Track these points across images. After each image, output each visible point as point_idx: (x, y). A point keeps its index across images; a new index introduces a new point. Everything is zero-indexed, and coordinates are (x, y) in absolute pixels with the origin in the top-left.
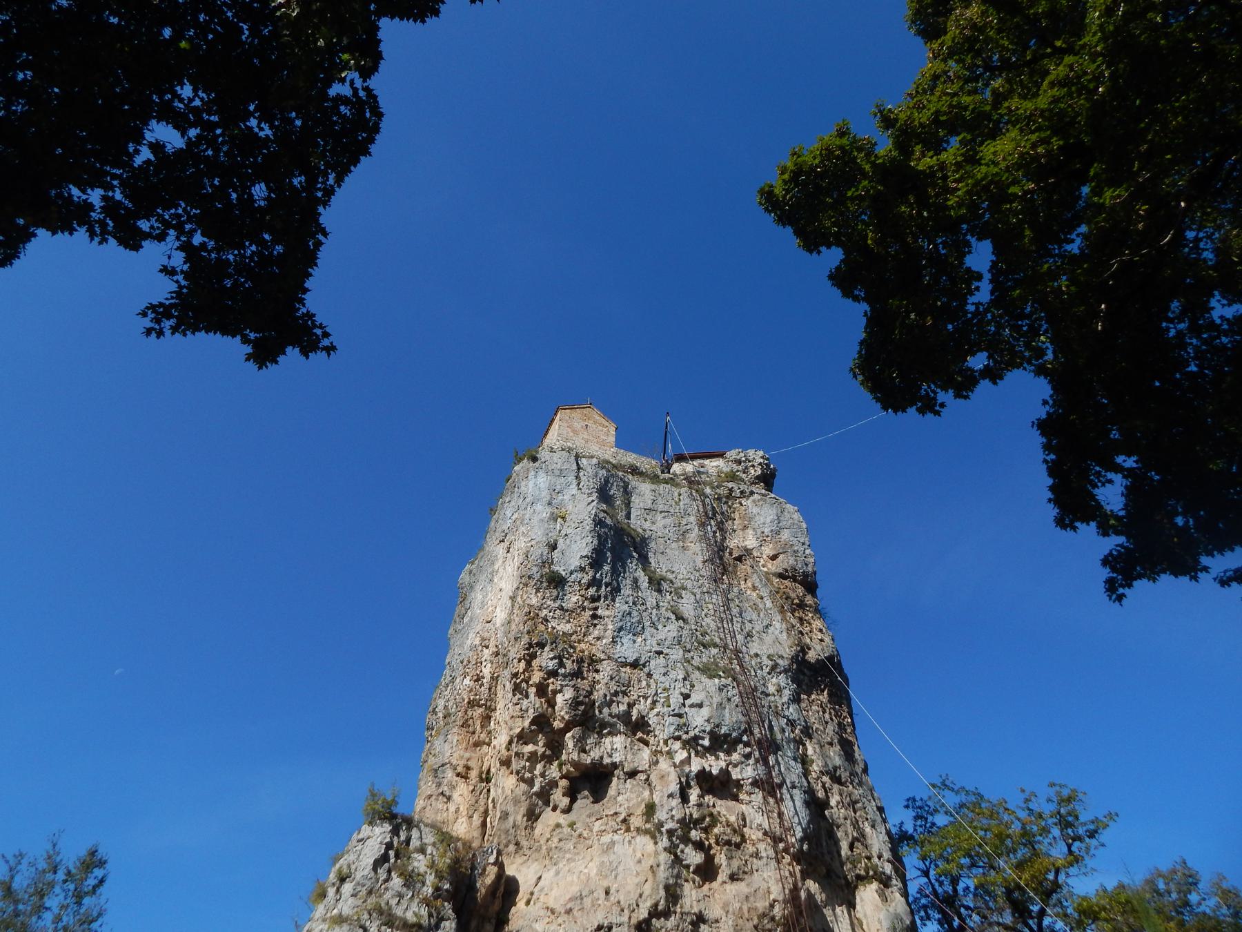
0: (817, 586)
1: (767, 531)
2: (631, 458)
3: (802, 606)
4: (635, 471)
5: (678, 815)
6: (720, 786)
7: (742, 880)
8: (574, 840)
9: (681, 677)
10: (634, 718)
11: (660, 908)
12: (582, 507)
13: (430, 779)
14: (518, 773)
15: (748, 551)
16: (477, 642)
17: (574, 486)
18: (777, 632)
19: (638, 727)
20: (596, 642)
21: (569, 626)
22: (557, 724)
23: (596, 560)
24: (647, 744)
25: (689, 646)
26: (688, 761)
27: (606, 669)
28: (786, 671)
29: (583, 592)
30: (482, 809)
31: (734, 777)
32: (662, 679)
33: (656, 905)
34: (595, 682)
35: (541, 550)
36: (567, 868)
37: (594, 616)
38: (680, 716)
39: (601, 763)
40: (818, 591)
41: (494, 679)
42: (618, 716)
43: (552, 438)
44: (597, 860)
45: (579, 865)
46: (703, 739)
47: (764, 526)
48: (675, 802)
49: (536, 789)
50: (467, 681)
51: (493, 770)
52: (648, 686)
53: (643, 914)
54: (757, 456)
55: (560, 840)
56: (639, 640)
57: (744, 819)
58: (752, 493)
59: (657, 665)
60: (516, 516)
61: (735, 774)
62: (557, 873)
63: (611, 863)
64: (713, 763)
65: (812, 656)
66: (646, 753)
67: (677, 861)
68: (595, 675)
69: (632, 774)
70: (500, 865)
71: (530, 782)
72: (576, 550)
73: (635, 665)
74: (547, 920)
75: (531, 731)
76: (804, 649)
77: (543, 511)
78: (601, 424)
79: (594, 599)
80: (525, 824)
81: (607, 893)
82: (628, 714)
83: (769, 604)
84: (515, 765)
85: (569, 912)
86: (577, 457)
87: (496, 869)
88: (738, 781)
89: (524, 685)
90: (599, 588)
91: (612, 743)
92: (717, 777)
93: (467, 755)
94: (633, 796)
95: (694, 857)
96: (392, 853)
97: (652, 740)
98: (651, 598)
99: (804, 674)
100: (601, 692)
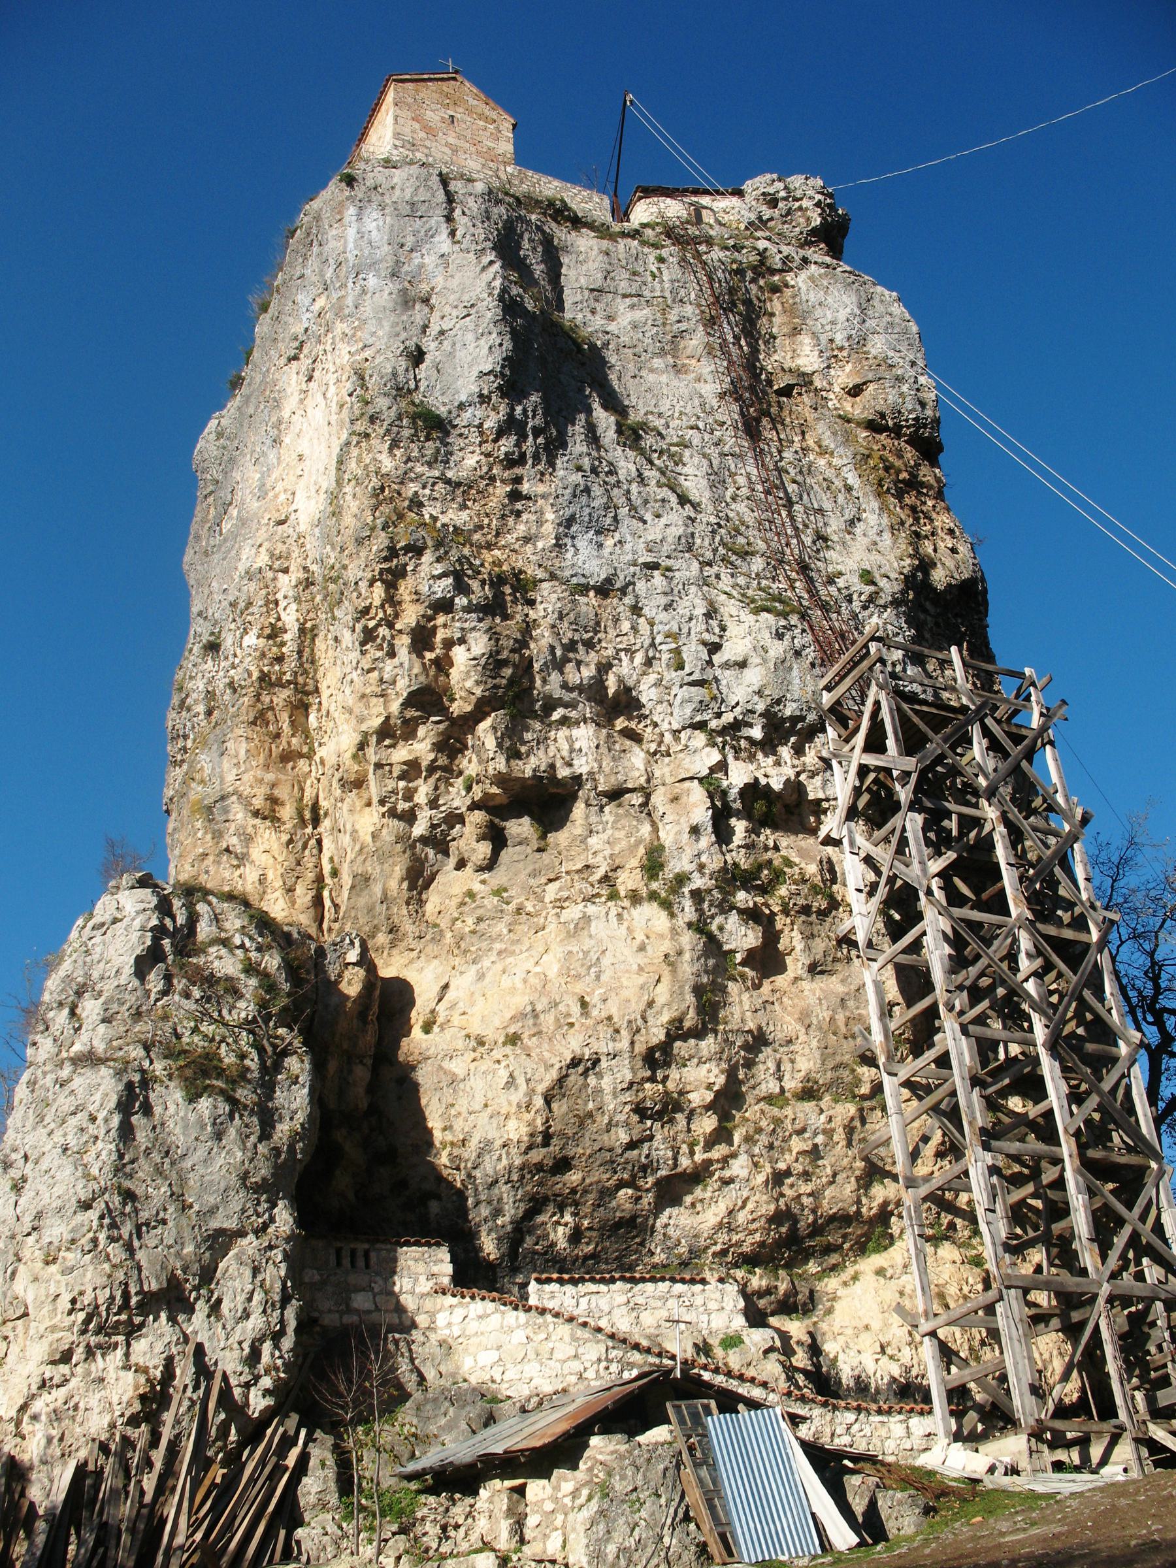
0: (940, 448)
1: (840, 338)
2: (549, 187)
3: (913, 484)
4: (561, 213)
5: (714, 862)
6: (790, 810)
7: (830, 973)
8: (508, 918)
9: (700, 611)
10: (611, 692)
11: (687, 1024)
12: (465, 282)
13: (199, 824)
14: (382, 802)
15: (805, 380)
16: (263, 560)
17: (444, 235)
18: (872, 533)
19: (617, 708)
20: (527, 543)
21: (464, 515)
22: (459, 707)
23: (513, 381)
24: (636, 738)
25: (709, 555)
26: (722, 766)
27: (549, 600)
28: (895, 603)
29: (488, 447)
30: (311, 876)
31: (811, 796)
32: (663, 616)
33: (680, 1020)
34: (528, 628)
35: (387, 360)
36: (499, 967)
37: (515, 496)
38: (701, 683)
39: (553, 777)
40: (942, 458)
41: (307, 633)
42: (580, 688)
43: (382, 138)
44: (558, 951)
45: (522, 963)
46: (751, 726)
47: (842, 330)
48: (707, 839)
49: (419, 829)
50: (251, 639)
51: (324, 804)
52: (635, 629)
53: (658, 1035)
54: (807, 189)
55: (480, 920)
56: (609, 542)
57: (832, 870)
58: (805, 260)
59: (650, 590)
60: (321, 302)
61: (814, 790)
62: (481, 977)
63: (586, 953)
64: (770, 771)
65: (939, 577)
66: (637, 758)
67: (712, 946)
68: (526, 609)
69: (616, 795)
70: (366, 962)
71: (409, 817)
72: (468, 358)
73: (604, 590)
74: (473, 1055)
75: (406, 722)
76: (925, 565)
77: (380, 291)
78: (482, 116)
79: (511, 462)
80: (405, 895)
81: (584, 1004)
82: (599, 683)
83: (853, 479)
84: (374, 789)
85: (513, 1040)
86: (444, 181)
87: (361, 973)
88: (818, 802)
89: (383, 631)
90: (522, 437)
91: (570, 740)
92: (779, 795)
93: (270, 777)
94: (621, 834)
95: (740, 937)
96: (166, 943)
97: (648, 733)
98: (626, 463)
99: (925, 611)
100: (544, 642)
